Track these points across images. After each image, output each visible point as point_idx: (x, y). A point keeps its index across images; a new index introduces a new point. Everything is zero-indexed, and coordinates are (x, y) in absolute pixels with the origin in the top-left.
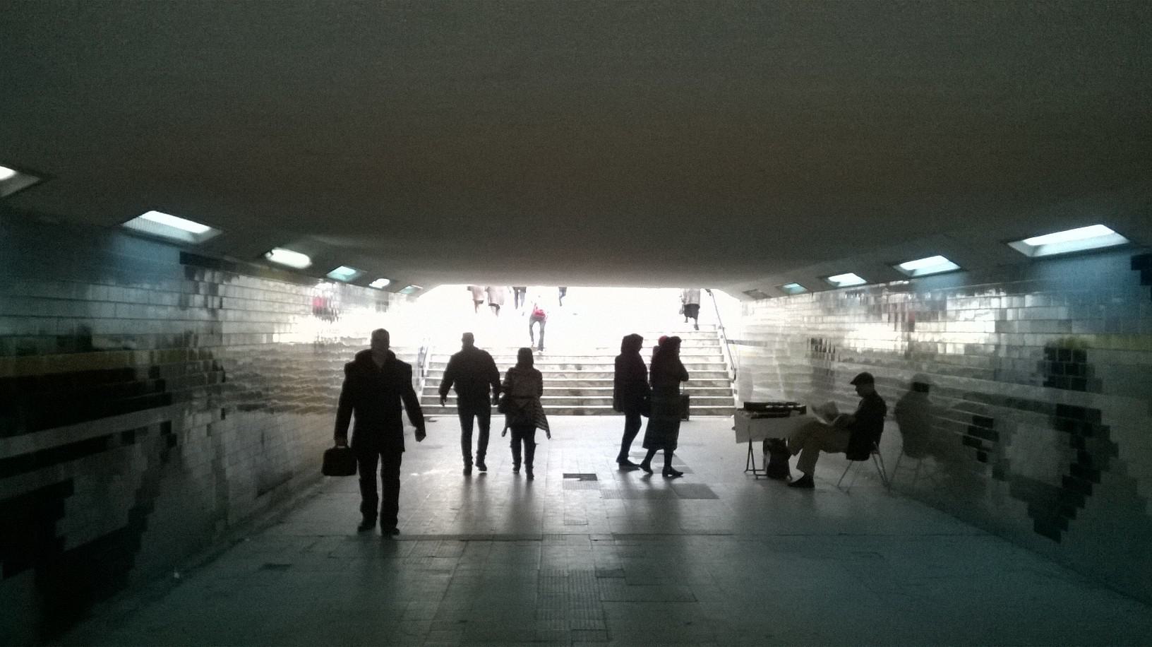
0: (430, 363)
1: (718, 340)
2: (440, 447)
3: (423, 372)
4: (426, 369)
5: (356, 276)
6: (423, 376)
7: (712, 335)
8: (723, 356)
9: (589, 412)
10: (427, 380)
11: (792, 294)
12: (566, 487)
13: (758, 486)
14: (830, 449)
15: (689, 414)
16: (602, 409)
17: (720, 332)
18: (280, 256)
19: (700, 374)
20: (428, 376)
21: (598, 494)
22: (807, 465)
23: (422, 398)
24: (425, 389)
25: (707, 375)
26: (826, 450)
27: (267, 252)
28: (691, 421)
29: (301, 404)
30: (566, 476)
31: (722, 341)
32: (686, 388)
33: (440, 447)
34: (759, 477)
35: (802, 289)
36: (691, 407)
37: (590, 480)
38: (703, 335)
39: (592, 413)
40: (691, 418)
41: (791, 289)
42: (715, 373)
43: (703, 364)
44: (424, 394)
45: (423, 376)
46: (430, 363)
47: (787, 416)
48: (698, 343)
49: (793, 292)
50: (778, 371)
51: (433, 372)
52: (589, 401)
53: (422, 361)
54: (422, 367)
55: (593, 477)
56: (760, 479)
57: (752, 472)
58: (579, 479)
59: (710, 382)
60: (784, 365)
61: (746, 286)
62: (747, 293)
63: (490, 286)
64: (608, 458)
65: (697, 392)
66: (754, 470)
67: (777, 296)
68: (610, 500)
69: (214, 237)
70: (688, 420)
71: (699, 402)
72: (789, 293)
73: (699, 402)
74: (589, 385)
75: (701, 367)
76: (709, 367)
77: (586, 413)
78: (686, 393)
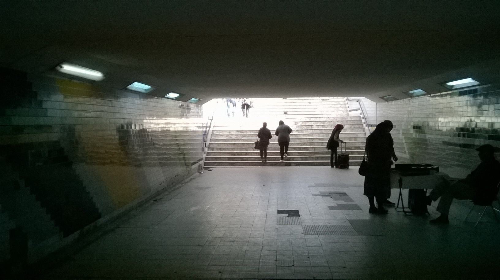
0: (211, 139)
1: (363, 125)
2: (208, 188)
3: (205, 144)
4: (207, 143)
5: (151, 90)
6: (205, 146)
7: (359, 122)
8: (365, 133)
9: (293, 165)
10: (208, 148)
11: (414, 97)
12: (279, 222)
13: (406, 221)
14: (460, 197)
15: (348, 165)
16: (301, 162)
17: (363, 121)
18: (137, 86)
19: (353, 143)
20: (209, 146)
21: (300, 229)
22: (444, 208)
23: (206, 158)
24: (207, 153)
25: (357, 143)
26: (457, 198)
27: (56, 66)
28: (350, 169)
29: (172, 156)
30: (280, 212)
31: (364, 125)
32: (346, 151)
33: (208, 188)
34: (407, 214)
35: (423, 92)
36: (349, 161)
37: (293, 215)
38: (354, 123)
39: (295, 165)
40: (350, 167)
41: (413, 93)
42: (362, 142)
43: (354, 138)
44: (207, 156)
45: (205, 146)
46: (211, 139)
47: (428, 174)
48: (296, 128)
49: (414, 95)
50: (404, 141)
51: (211, 143)
52: (293, 159)
53: (205, 138)
54: (205, 142)
55: (295, 213)
56: (408, 215)
57: (402, 210)
58: (288, 215)
59: (359, 147)
60: (409, 137)
61: (382, 94)
62: (382, 98)
63: (248, 101)
64: (305, 196)
65: (352, 153)
66: (403, 208)
67: (403, 98)
68: (309, 236)
69: (151, 91)
70: (348, 169)
71: (353, 158)
72: (412, 96)
73: (353, 158)
74: (293, 150)
75: (353, 139)
76: (358, 139)
77: (292, 165)
78: (348, 154)
